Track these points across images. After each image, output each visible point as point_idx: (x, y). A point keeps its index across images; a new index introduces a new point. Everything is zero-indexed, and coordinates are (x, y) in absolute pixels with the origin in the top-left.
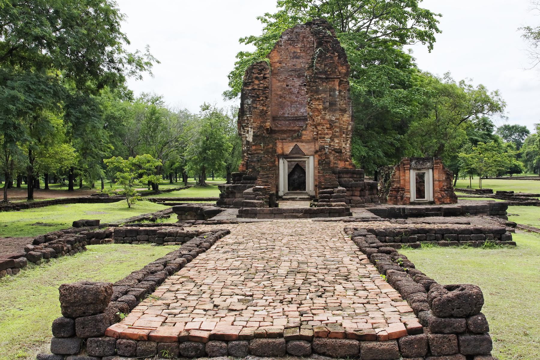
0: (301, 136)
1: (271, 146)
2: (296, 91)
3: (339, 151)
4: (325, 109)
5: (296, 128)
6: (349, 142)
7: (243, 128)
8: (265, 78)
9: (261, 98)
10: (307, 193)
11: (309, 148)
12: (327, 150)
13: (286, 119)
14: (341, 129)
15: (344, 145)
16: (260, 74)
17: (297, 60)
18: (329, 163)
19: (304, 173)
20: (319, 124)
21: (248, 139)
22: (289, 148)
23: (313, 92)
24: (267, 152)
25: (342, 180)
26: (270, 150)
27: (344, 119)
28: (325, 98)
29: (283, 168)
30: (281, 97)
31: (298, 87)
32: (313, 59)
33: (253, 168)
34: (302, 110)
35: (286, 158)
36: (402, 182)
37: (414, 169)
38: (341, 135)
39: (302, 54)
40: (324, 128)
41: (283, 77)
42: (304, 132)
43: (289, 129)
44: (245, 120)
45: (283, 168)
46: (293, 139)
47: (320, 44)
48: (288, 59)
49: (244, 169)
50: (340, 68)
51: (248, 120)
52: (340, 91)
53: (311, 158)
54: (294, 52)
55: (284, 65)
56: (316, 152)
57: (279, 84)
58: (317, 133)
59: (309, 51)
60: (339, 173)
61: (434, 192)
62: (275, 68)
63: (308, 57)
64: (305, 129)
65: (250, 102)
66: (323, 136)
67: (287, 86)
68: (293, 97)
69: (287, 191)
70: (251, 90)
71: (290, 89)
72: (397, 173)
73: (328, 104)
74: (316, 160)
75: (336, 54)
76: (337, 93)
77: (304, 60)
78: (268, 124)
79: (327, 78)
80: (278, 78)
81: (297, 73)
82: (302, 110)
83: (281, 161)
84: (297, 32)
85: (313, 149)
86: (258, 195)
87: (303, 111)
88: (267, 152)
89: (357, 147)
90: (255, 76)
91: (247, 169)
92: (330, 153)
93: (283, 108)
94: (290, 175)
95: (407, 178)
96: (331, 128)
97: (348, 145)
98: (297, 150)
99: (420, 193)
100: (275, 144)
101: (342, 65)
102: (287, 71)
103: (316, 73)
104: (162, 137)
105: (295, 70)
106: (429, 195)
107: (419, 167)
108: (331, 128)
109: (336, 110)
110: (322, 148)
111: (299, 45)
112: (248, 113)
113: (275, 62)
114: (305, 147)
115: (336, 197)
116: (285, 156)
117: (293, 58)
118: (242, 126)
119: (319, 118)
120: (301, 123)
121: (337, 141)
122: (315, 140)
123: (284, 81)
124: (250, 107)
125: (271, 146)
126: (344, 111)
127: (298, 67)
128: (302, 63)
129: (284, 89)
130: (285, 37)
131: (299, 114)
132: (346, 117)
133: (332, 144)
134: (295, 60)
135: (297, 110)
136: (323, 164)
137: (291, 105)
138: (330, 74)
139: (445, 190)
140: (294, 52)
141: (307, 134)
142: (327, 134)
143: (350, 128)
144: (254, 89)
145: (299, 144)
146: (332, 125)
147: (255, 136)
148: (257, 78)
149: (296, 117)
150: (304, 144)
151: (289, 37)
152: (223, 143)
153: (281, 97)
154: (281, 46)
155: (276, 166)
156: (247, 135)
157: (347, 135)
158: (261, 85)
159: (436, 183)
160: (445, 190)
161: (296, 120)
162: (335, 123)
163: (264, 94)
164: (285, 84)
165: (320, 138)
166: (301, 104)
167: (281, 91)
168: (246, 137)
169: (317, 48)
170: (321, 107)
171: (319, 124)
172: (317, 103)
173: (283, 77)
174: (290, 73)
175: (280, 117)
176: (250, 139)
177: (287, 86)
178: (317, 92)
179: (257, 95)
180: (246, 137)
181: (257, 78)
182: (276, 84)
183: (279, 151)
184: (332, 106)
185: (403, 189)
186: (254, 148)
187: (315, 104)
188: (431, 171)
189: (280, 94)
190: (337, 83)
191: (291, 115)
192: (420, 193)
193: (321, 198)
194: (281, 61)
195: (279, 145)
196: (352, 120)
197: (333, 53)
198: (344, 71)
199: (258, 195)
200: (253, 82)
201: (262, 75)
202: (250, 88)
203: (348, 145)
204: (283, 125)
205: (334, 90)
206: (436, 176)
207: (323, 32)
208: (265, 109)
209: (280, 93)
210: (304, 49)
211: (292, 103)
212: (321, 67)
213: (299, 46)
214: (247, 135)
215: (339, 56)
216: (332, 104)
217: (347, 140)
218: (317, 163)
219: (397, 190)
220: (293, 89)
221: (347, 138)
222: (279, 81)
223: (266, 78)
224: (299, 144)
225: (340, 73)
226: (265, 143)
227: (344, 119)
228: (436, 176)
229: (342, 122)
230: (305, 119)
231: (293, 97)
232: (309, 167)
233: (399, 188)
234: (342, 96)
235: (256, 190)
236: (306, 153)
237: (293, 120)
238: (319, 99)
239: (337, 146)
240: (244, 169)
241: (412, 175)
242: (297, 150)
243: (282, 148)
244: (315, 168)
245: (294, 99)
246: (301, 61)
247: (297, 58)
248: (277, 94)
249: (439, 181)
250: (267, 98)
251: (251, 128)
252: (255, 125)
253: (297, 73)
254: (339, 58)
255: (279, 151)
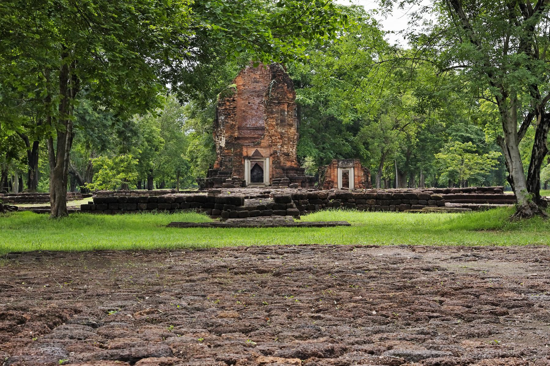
0: (260, 143)
1: (239, 150)
2: (256, 107)
3: (287, 155)
4: (277, 124)
5: (256, 136)
8: (234, 100)
12: (278, 154)
13: (248, 129)
14: (289, 138)
15: (291, 150)
16: (230, 98)
18: (280, 163)
19: (263, 171)
20: (273, 135)
22: (251, 152)
23: (269, 112)
24: (236, 155)
25: (289, 175)
26: (238, 153)
27: (292, 131)
28: (277, 117)
29: (248, 166)
30: (244, 112)
32: (269, 88)
33: (226, 166)
34: (260, 122)
35: (249, 159)
36: (332, 177)
37: (341, 168)
38: (289, 143)
39: (260, 80)
40: (276, 138)
41: (246, 96)
42: (262, 141)
45: (248, 166)
46: (255, 146)
47: (274, 77)
49: (218, 167)
50: (288, 95)
51: (221, 131)
52: (288, 112)
53: (268, 159)
54: (255, 78)
55: (247, 87)
56: (271, 155)
57: (243, 102)
59: (266, 78)
60: (287, 169)
61: (355, 184)
62: (240, 90)
63: (266, 82)
64: (263, 139)
65: (223, 118)
66: (276, 144)
67: (249, 103)
68: (254, 112)
69: (250, 183)
72: (329, 170)
74: (271, 161)
75: (286, 84)
76: (286, 113)
77: (262, 84)
78: (236, 134)
79: (279, 103)
80: (242, 97)
81: (257, 94)
82: (260, 122)
83: (246, 161)
85: (268, 153)
86: (235, 181)
87: (261, 123)
88: (236, 155)
89: (309, 149)
90: (226, 99)
91: (221, 167)
92: (281, 156)
93: (245, 120)
94: (252, 171)
95: (336, 174)
96: (281, 138)
97: (294, 150)
98: (257, 153)
99: (346, 184)
100: (242, 149)
101: (290, 92)
102: (249, 92)
103: (271, 99)
105: (255, 92)
107: (344, 166)
108: (281, 138)
109: (285, 125)
110: (275, 152)
111: (259, 73)
114: (263, 152)
115: (282, 183)
117: (254, 82)
119: (273, 131)
120: (260, 132)
122: (270, 146)
123: (246, 99)
124: (223, 122)
125: (239, 150)
126: (291, 125)
127: (258, 89)
128: (260, 87)
129: (247, 105)
131: (258, 125)
132: (293, 130)
134: (255, 84)
135: (256, 122)
136: (276, 164)
138: (281, 100)
139: (362, 183)
140: (255, 78)
141: (265, 142)
142: (279, 142)
143: (295, 138)
144: (226, 109)
145: (259, 149)
146: (282, 136)
147: (227, 143)
148: (228, 101)
150: (262, 149)
152: (154, 137)
153: (244, 112)
155: (242, 165)
156: (220, 142)
158: (231, 106)
159: (356, 177)
160: (362, 183)
163: (234, 112)
166: (260, 118)
169: (272, 79)
170: (274, 123)
171: (273, 135)
172: (272, 120)
173: (246, 96)
177: (249, 103)
178: (272, 113)
181: (228, 101)
182: (241, 102)
183: (245, 154)
184: (282, 122)
185: (333, 182)
186: (226, 151)
187: (270, 121)
188: (352, 169)
190: (286, 106)
192: (346, 184)
193: (274, 183)
195: (245, 150)
196: (297, 132)
197: (284, 84)
198: (291, 97)
199: (235, 181)
200: (225, 104)
202: (223, 108)
203: (294, 150)
204: (247, 134)
205: (284, 111)
206: (356, 173)
207: (276, 67)
208: (234, 123)
210: (262, 76)
212: (275, 95)
213: (259, 73)
214: (220, 142)
215: (287, 86)
216: (282, 121)
218: (271, 163)
219: (329, 182)
222: (243, 100)
223: (235, 100)
224: (259, 149)
226: (234, 149)
227: (292, 131)
228: (356, 173)
230: (263, 129)
231: (254, 112)
233: (330, 181)
235: (233, 179)
236: (263, 156)
238: (273, 117)
239: (286, 151)
240: (218, 167)
241: (340, 172)
242: (257, 153)
243: (247, 152)
244: (270, 166)
247: (257, 82)
248: (241, 110)
249: (358, 176)
250: (235, 115)
252: (227, 135)
253: (257, 94)
254: (288, 88)
255: (245, 154)
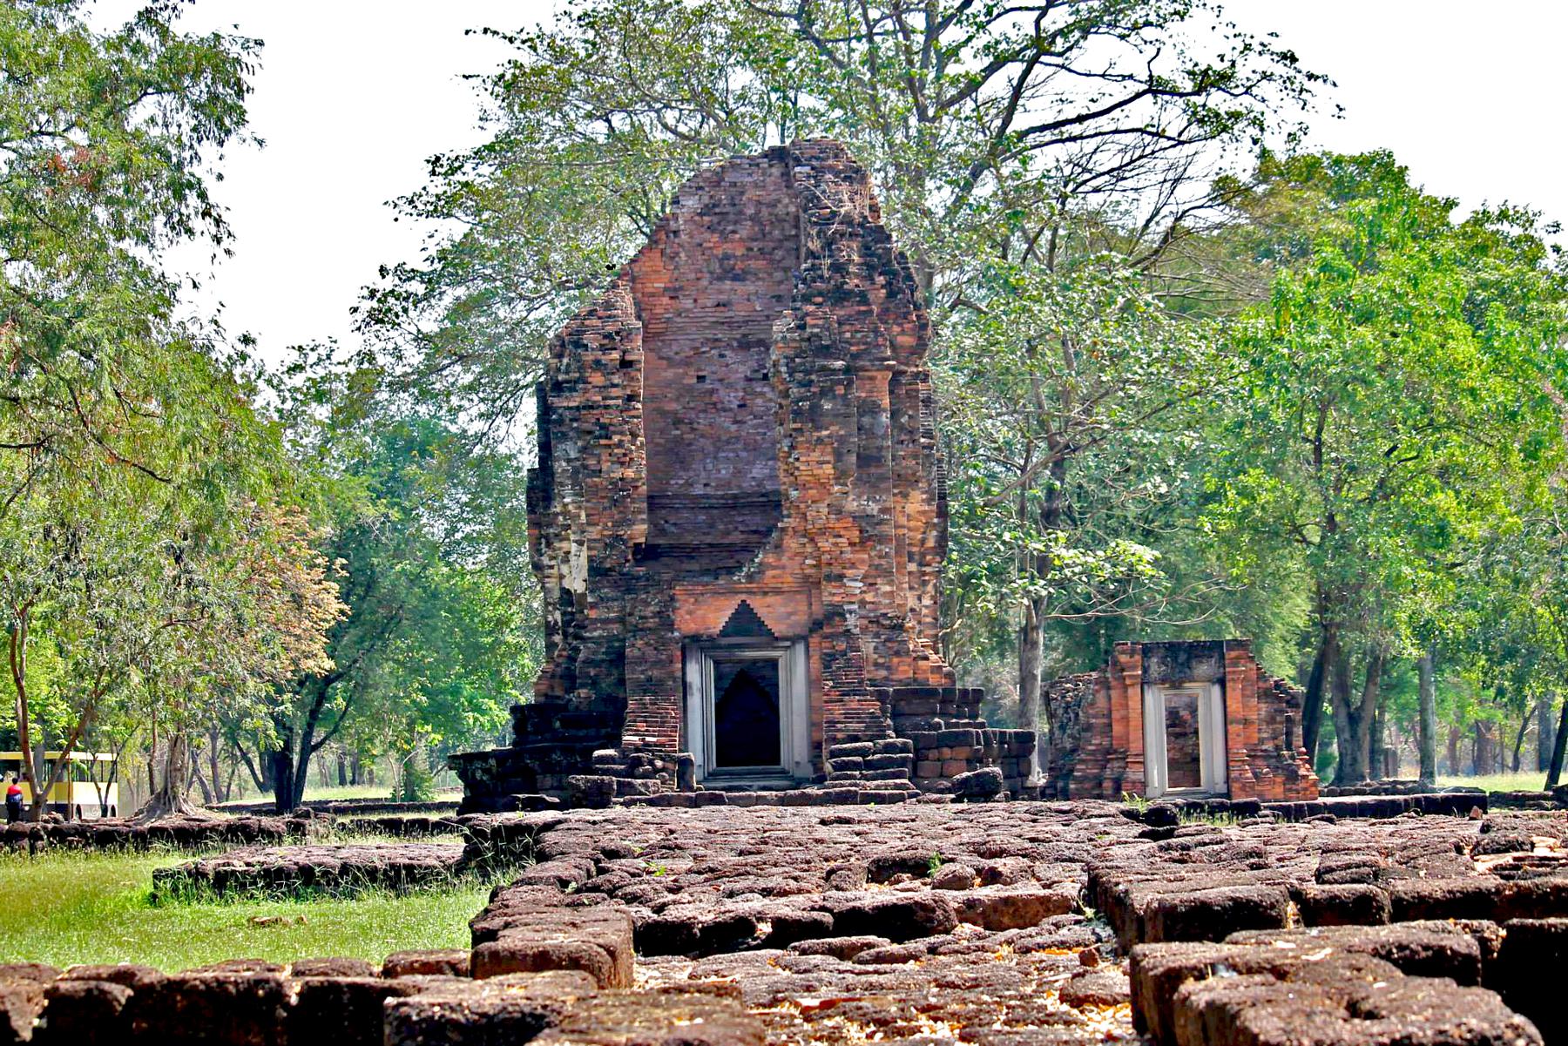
2: (732, 399)
5: (736, 538)
6: (930, 588)
7: (549, 545)
8: (625, 364)
9: (616, 439)
10: (784, 772)
11: (790, 614)
12: (851, 620)
13: (697, 504)
15: (912, 602)
17: (738, 285)
20: (823, 531)
21: (566, 584)
30: (677, 422)
31: (742, 384)
39: (753, 264)
43: (709, 539)
44: (557, 514)
48: (705, 282)
55: (689, 303)
57: (670, 374)
58: (818, 559)
59: (779, 254)
66: (836, 570)
67: (701, 379)
68: (725, 421)
70: (578, 408)
71: (712, 392)
73: (853, 458)
76: (885, 418)
78: (639, 531)
80: (666, 352)
81: (737, 334)
84: (735, 185)
93: (684, 464)
96: (864, 541)
98: (745, 621)
104: (646, 604)
106: (1212, 769)
112: (568, 490)
113: (653, 295)
114: (776, 613)
116: (696, 644)
118: (547, 537)
121: (888, 588)
123: (686, 363)
124: (576, 471)
130: (691, 203)
131: (748, 485)
133: (869, 597)
134: (728, 284)
137: (718, 449)
142: (853, 565)
146: (868, 532)
147: (597, 571)
149: (735, 497)
150: (770, 599)
151: (706, 200)
153: (677, 422)
154: (676, 233)
157: (920, 565)
158: (615, 392)
161: (734, 507)
162: (881, 522)
164: (692, 372)
165: (829, 578)
167: (677, 400)
168: (562, 577)
171: (823, 531)
174: (709, 334)
175: (676, 496)
176: (577, 585)
177: (701, 379)
179: (603, 427)
180: (562, 577)
189: (675, 413)
191: (717, 488)
194: (675, 290)
201: (616, 355)
203: (927, 601)
205: (874, 409)
209: (674, 406)
211: (720, 444)
214: (565, 569)
217: (925, 583)
220: (722, 393)
221: (924, 574)
223: (630, 364)
225: (893, 346)
229: (903, 521)
231: (725, 421)
232: (789, 683)
234: (902, 428)
236: (778, 629)
237: (725, 506)
241: (1156, 703)
242: (745, 621)
245: (727, 431)
246: (752, 288)
247: (736, 278)
251: (580, 543)
252: (593, 533)
